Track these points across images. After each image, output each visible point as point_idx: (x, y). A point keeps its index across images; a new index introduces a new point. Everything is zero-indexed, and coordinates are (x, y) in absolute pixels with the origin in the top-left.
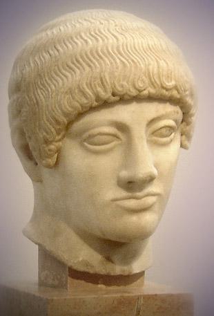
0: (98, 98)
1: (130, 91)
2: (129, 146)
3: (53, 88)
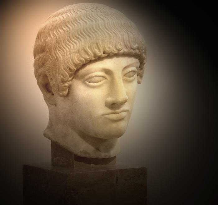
0: (95, 55)
1: (113, 50)
2: (112, 84)
3: (68, 50)
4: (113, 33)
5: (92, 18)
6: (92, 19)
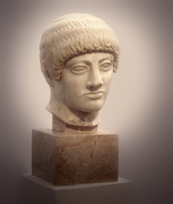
1: (91, 48)
2: (91, 71)
4: (91, 35)
5: (78, 24)
6: (78, 25)
